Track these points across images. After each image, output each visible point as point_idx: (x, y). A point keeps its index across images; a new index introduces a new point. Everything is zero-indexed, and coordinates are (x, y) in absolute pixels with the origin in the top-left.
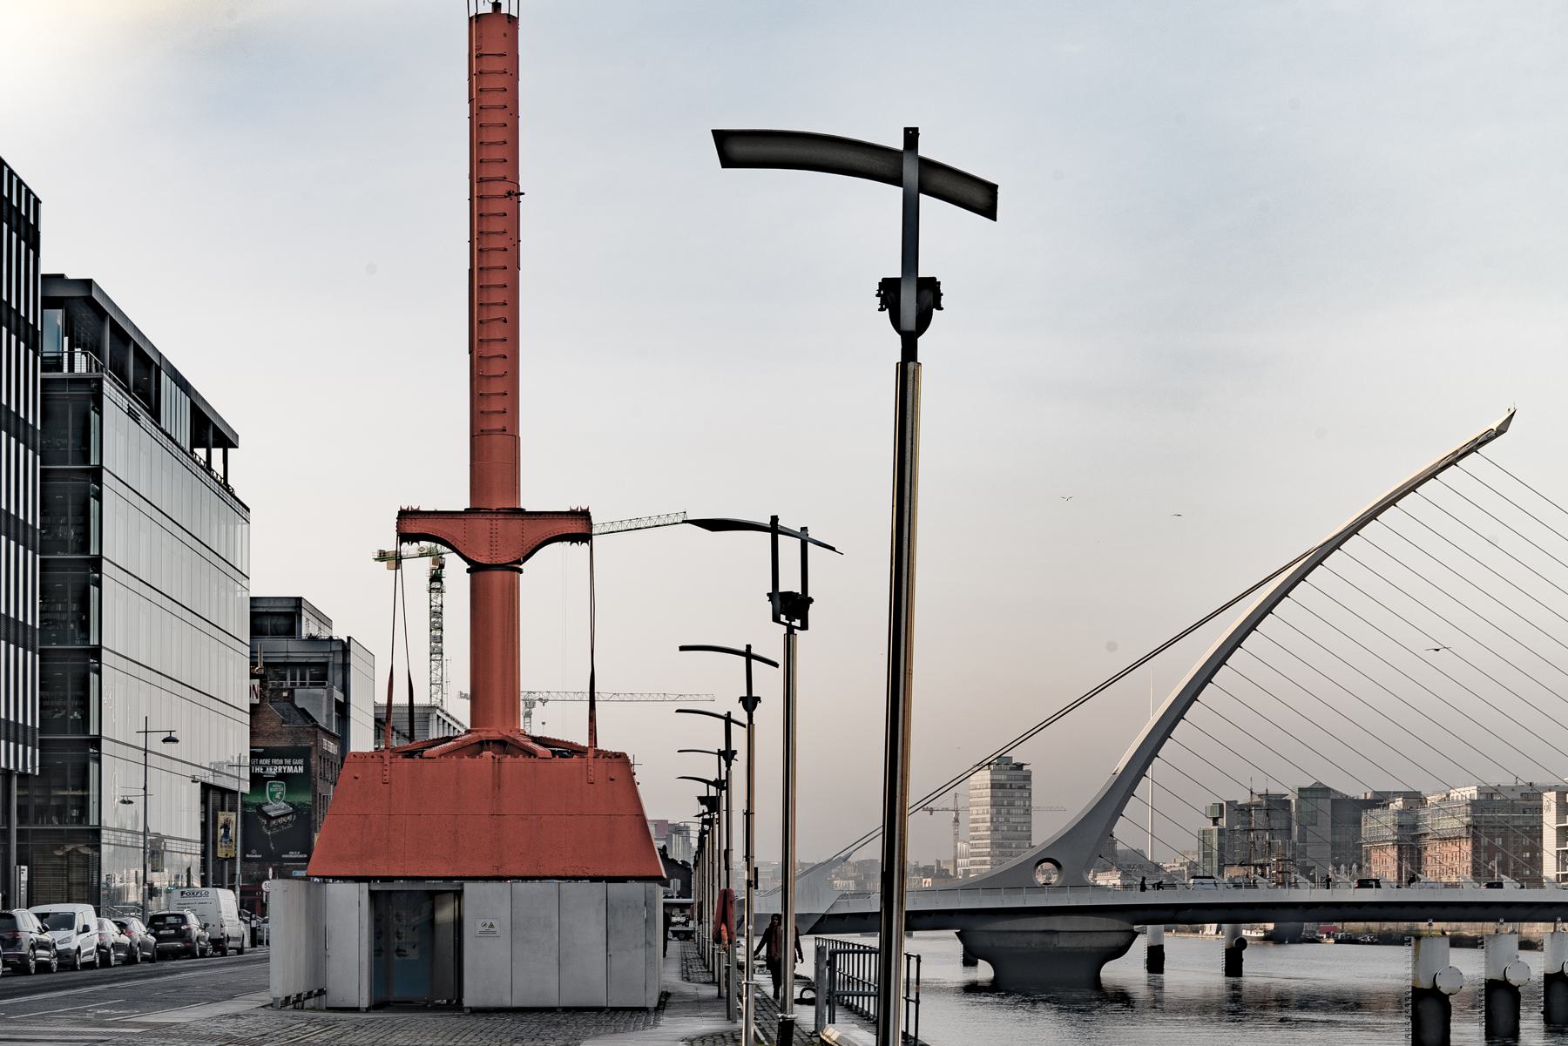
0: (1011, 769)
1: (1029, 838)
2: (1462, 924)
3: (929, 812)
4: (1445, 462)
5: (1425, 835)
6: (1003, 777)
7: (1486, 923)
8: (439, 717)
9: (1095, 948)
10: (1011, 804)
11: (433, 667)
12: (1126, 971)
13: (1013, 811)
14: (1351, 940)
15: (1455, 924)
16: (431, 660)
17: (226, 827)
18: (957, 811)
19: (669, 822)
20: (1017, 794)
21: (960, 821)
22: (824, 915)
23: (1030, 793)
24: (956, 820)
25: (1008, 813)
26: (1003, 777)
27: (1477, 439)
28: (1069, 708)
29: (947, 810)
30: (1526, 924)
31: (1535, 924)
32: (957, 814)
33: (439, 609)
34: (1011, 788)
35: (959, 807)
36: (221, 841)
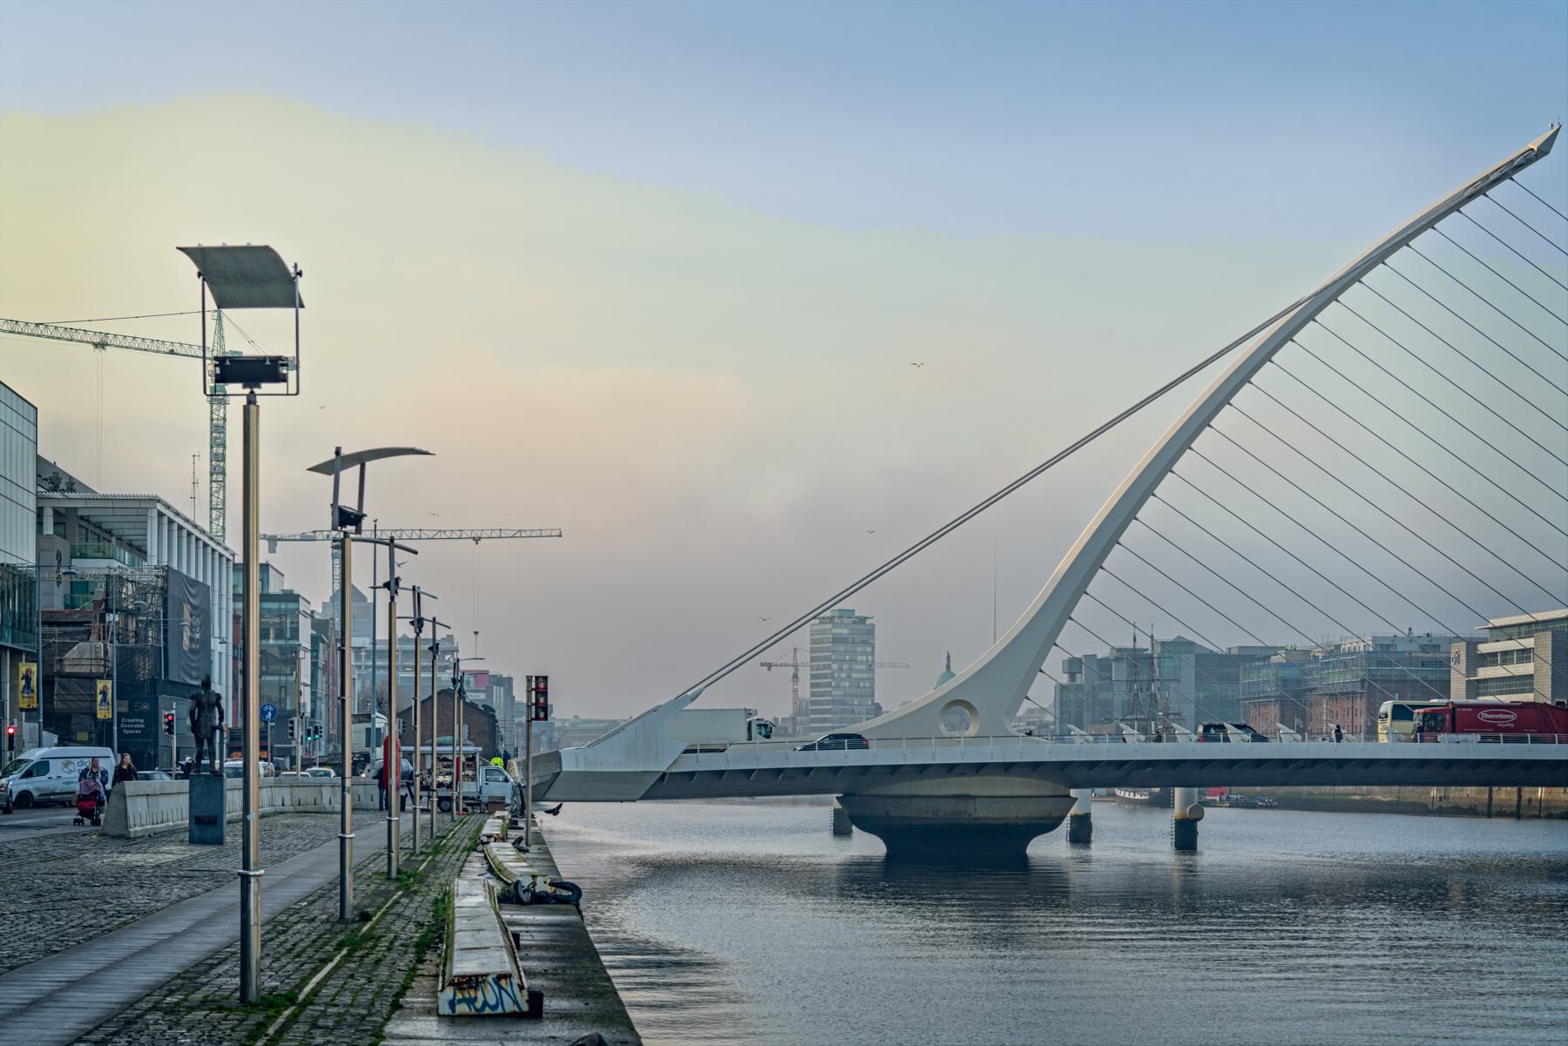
0: (854, 622)
1: (872, 695)
2: (1374, 787)
3: (766, 668)
4: (1472, 190)
5: (1311, 690)
6: (845, 631)
7: (1403, 788)
8: (161, 515)
9: (1022, 818)
10: (854, 660)
11: (214, 489)
12: (1049, 848)
13: (856, 667)
14: (1249, 805)
15: (1365, 788)
16: (211, 481)
17: (104, 693)
18: (796, 666)
19: (490, 674)
20: (859, 649)
21: (799, 676)
22: (664, 774)
23: (873, 648)
24: (795, 676)
25: (851, 669)
26: (845, 631)
27: (1512, 161)
28: (945, 530)
29: (786, 665)
30: (1453, 788)
31: (1465, 788)
32: (797, 669)
33: (221, 422)
34: (853, 642)
35: (799, 662)
36: (23, 692)
